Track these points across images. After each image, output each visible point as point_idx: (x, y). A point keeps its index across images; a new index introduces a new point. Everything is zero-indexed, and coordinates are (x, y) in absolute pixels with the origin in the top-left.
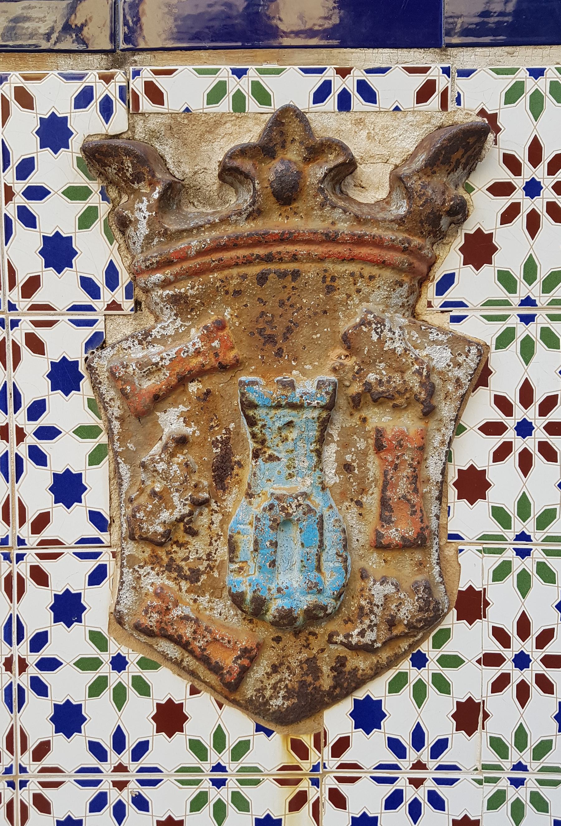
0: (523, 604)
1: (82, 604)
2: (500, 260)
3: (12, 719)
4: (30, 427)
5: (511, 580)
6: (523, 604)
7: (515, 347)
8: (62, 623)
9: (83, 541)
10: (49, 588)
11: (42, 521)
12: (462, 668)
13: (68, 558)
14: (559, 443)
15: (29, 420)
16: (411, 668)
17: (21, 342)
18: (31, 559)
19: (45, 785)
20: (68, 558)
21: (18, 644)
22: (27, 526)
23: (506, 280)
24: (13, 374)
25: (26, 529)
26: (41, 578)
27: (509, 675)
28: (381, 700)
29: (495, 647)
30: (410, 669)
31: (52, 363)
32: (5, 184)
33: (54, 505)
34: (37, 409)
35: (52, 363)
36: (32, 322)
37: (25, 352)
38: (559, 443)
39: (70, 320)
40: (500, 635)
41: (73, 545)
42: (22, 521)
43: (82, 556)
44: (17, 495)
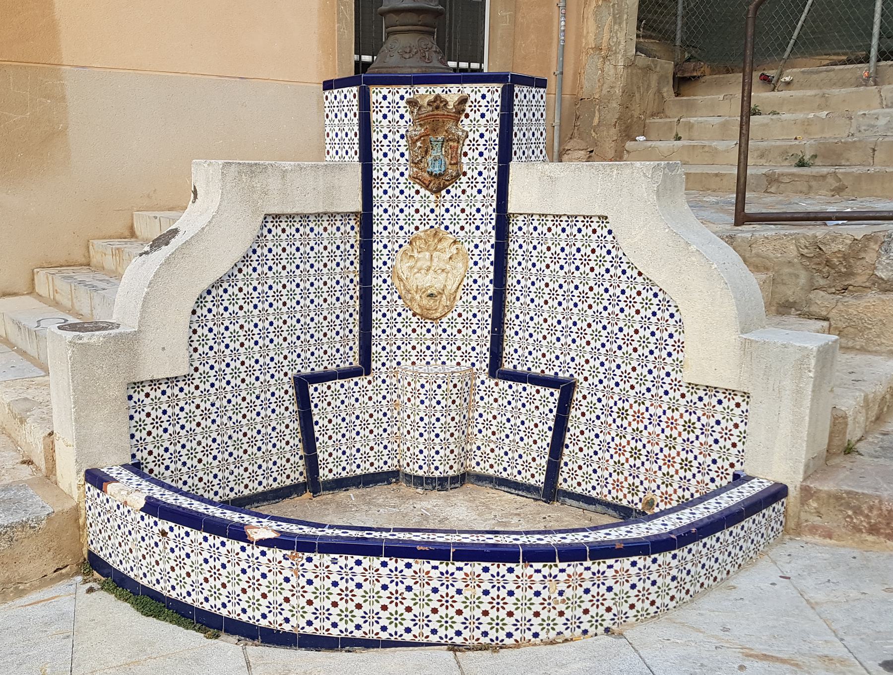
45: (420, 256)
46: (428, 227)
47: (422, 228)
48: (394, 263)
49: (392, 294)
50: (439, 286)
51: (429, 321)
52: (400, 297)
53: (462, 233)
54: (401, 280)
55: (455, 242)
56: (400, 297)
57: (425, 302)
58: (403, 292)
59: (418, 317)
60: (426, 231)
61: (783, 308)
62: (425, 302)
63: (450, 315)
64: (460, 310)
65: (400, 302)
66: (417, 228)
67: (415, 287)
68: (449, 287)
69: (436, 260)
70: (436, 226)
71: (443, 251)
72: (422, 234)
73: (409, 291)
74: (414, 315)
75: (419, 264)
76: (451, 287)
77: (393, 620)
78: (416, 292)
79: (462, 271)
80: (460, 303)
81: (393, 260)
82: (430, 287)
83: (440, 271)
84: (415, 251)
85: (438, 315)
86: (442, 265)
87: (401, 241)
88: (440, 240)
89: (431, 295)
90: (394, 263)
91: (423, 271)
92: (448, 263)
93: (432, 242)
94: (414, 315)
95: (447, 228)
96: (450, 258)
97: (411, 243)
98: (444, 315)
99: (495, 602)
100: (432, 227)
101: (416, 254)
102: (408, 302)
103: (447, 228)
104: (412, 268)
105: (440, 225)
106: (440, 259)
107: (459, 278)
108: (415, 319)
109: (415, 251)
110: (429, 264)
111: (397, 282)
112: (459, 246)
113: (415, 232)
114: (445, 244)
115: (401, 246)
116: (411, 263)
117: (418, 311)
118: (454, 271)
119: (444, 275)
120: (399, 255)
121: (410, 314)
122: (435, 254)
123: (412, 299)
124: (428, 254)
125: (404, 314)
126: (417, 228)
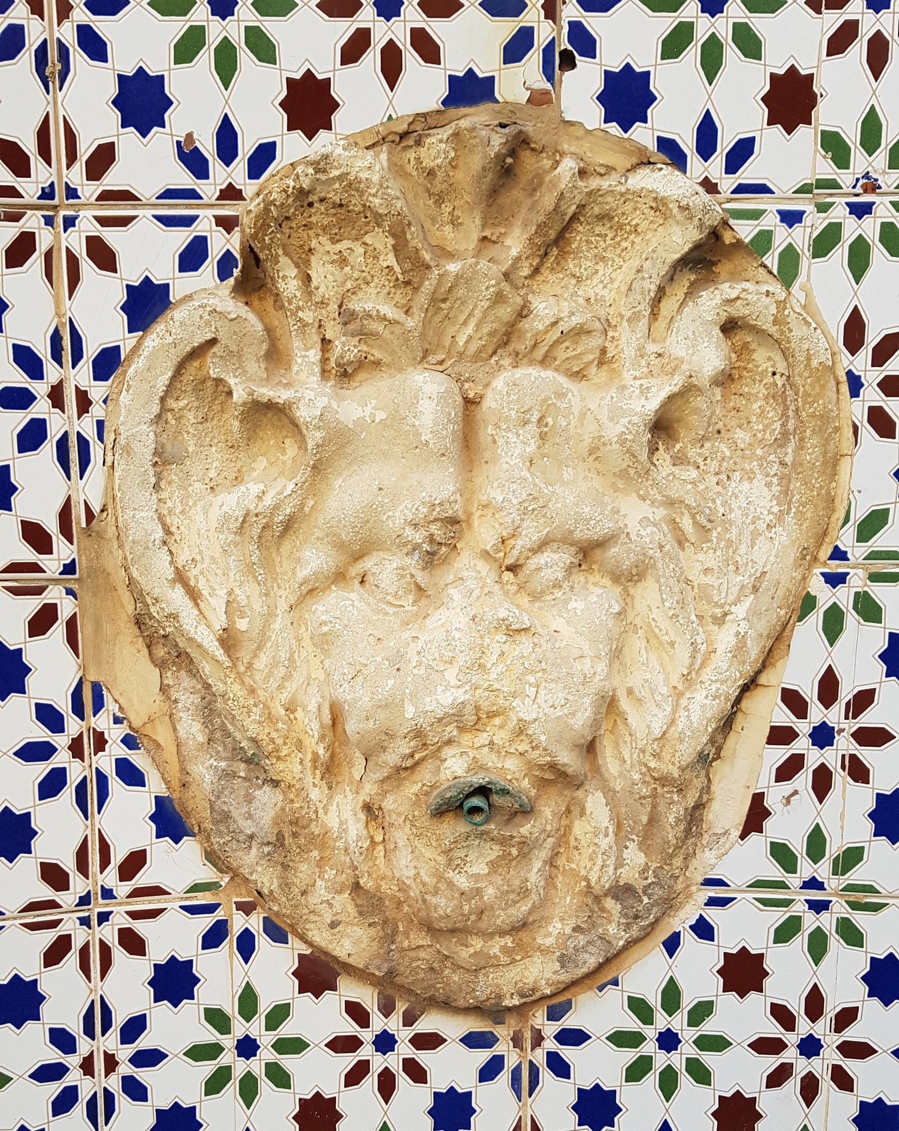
0: (829, 654)
1: (194, 975)
2: (825, 115)
3: (92, 991)
4: (125, 1053)
5: (800, 942)
6: (829, 654)
7: (840, 254)
8: (166, 1002)
9: (169, 194)
10: (147, 957)
11: (103, 159)
12: (728, 1053)
13: (147, 188)
14: (898, 408)
15: (95, 379)
16: (658, 1050)
17: (81, 251)
18: (87, 225)
19: (104, 222)
20: (147, 188)
21: (103, 1034)
22: (80, 167)
23: (834, 147)
24: (100, 984)
25: (79, 170)
26: (104, 257)
27: (802, 756)
28: (615, 1091)
29: (774, 1030)
30: (655, 1053)
31: (128, 287)
32: (43, 19)
33: (121, 131)
34: (135, 1027)
35: (128, 287)
36: (97, 218)
37: (87, 267)
38: (898, 408)
39: (157, 217)
40: (782, 1015)
41: (153, 200)
42: (72, 157)
43: (168, 221)
44: (61, 112)
45: (359, 406)
46: (424, 87)
47: (361, 97)
48: (90, 489)
49: (91, 796)
50: (550, 710)
51: (452, 1027)
52: (169, 822)
53: (786, 159)
54: (168, 651)
55: (707, 257)
56: (169, 822)
57: (415, 861)
58: (205, 772)
59: (350, 989)
60: (405, 136)
61: (572, 750)
62: (415, 861)
63: (646, 975)
64: (745, 926)
65: (177, 865)
66: (309, 104)
67: (310, 725)
68: (644, 720)
69: (510, 450)
70: (517, 82)
71: (582, 352)
72: (370, 167)
73: (253, 763)
74: (315, 976)
75: (347, 496)
76: (667, 710)
77: (817, 714)
78: (329, 770)
79: (773, 551)
80: (748, 861)
81: (74, 456)
82: (469, 720)
83: (552, 563)
84: (305, 357)
85: (540, 972)
86: (578, 500)
87: (145, 250)
88: (555, 241)
89: (476, 804)
90: (90, 489)
91: (388, 569)
92: (633, 476)
93: (473, 257)
94: (315, 976)
95: (627, 97)
96: (662, 427)
97: (249, 275)
98: (602, 976)
99: (822, 1029)
100: (469, 90)
101: (307, 391)
102: (249, 860)
103: (627, 97)
104: (275, 531)
105: (557, 62)
106: (559, 438)
107: (742, 626)
108: (320, 1017)
109: (305, 357)
110: (439, 485)
111: (134, 682)
112: (747, 290)
113: (293, 147)
114: (607, 280)
115: (145, 304)
116: (269, 480)
117: (351, 943)
118: (697, 562)
119: (595, 598)
120: (131, 406)
121: (273, 971)
122: (509, 387)
123: (291, 838)
124: (426, 394)
125: (219, 977)
126: (309, 104)
